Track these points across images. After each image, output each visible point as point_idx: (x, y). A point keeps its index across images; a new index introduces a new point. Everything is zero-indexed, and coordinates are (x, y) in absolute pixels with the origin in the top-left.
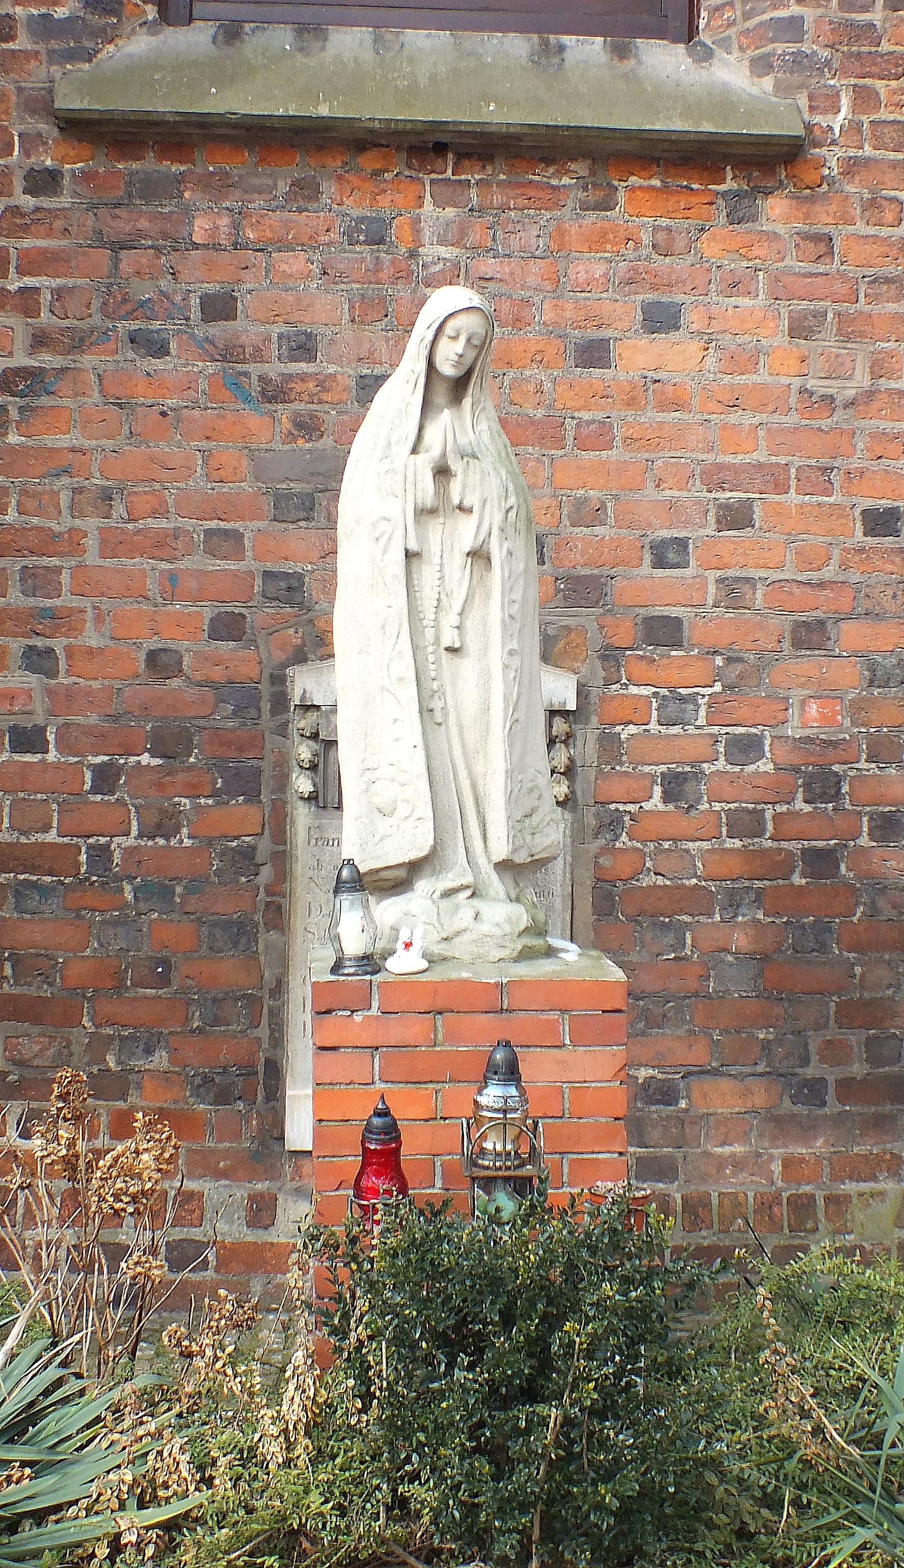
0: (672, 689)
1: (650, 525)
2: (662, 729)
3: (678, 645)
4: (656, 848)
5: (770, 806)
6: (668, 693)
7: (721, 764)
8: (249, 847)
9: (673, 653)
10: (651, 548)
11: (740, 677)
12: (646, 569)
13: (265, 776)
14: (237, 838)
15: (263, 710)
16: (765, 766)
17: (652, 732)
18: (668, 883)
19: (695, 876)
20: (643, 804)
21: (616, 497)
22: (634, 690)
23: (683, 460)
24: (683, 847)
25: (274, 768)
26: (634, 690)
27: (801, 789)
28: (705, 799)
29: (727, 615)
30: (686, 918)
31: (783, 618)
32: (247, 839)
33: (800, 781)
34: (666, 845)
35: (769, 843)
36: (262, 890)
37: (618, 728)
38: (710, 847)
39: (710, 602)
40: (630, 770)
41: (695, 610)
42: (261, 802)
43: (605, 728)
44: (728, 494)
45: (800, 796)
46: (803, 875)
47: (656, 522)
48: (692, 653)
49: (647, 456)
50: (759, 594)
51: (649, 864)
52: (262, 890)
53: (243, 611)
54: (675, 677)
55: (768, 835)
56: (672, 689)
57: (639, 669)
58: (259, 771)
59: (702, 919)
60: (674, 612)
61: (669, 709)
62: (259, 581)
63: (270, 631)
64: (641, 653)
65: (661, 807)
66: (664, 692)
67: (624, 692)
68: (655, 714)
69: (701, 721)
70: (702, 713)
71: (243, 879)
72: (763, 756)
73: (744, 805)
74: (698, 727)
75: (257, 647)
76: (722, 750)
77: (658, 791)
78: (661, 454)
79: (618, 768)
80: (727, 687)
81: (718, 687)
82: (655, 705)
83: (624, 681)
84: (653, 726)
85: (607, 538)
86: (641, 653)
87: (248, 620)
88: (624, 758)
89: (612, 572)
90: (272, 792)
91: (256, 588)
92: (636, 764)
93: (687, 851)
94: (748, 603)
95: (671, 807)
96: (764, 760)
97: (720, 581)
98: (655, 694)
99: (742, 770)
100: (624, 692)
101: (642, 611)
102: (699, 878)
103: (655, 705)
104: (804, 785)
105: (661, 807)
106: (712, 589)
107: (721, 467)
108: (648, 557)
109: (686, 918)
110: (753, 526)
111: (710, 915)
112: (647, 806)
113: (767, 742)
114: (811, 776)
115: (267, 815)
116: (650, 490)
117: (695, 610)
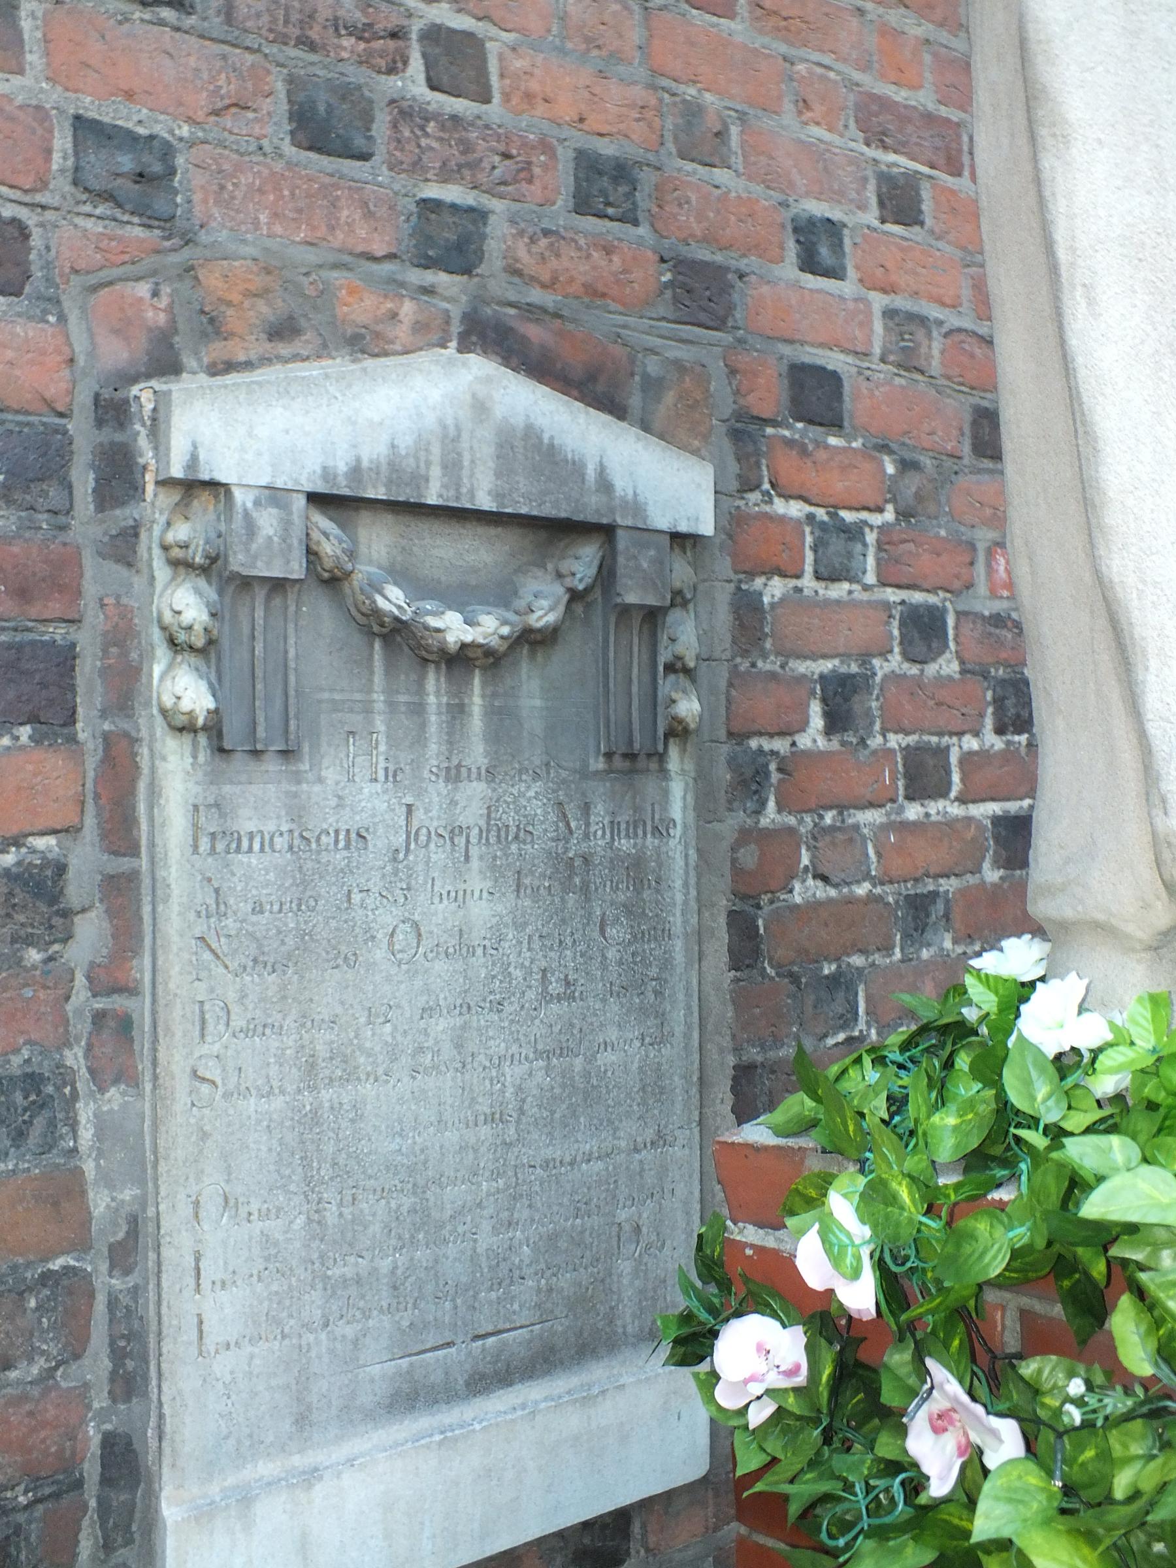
0: (833, 509)
1: (791, 184)
2: (820, 586)
3: (835, 424)
4: (816, 825)
5: (955, 739)
6: (826, 518)
7: (895, 663)
8: (46, 863)
9: (833, 441)
10: (796, 230)
11: (918, 497)
12: (789, 269)
13: (87, 669)
14: (17, 842)
15: (78, 493)
16: (947, 666)
17: (806, 592)
18: (833, 892)
19: (867, 876)
20: (797, 738)
21: (742, 117)
22: (780, 506)
23: (832, 75)
24: (850, 821)
25: (105, 651)
26: (780, 506)
27: (990, 710)
28: (877, 727)
29: (898, 380)
30: (857, 960)
31: (961, 397)
32: (41, 843)
33: (989, 695)
34: (829, 818)
35: (956, 810)
36: (80, 980)
37: (759, 582)
38: (884, 819)
39: (877, 350)
40: (777, 668)
41: (858, 363)
42: (72, 739)
43: (740, 581)
44: (892, 157)
45: (989, 723)
46: (997, 864)
47: (800, 182)
48: (854, 445)
49: (783, 48)
50: (937, 346)
51: (805, 860)
52: (80, 980)
53: (23, 213)
54: (839, 486)
55: (953, 795)
56: (833, 509)
57: (787, 463)
58: (67, 657)
59: (877, 958)
60: (835, 361)
61: (832, 549)
62: (62, 141)
63: (92, 280)
64: (787, 433)
65: (822, 743)
66: (821, 514)
67: (767, 508)
68: (809, 556)
69: (870, 578)
70: (871, 562)
71: (34, 956)
72: (946, 646)
73: (926, 738)
74: (866, 588)
75: (62, 318)
76: (896, 632)
77: (815, 710)
78: (802, 52)
79: (760, 664)
80: (904, 514)
81: (889, 515)
82: (809, 540)
83: (766, 486)
84: (808, 582)
85: (733, 194)
86: (787, 433)
87: (36, 241)
88: (768, 645)
89: (743, 264)
90: (104, 714)
91: (56, 157)
92: (787, 654)
93: (856, 827)
94: (922, 363)
95: (835, 745)
96: (947, 655)
97: (889, 314)
98: (811, 518)
99: (922, 671)
100: (767, 508)
101: (786, 350)
102: (876, 881)
103: (809, 540)
104: (995, 701)
105: (822, 743)
106: (878, 326)
107: (885, 103)
108: (792, 249)
109: (857, 960)
110: (922, 224)
111: (887, 949)
112: (804, 741)
113: (951, 621)
114: (1003, 682)
115: (91, 774)
116: (789, 116)
117: (858, 363)
